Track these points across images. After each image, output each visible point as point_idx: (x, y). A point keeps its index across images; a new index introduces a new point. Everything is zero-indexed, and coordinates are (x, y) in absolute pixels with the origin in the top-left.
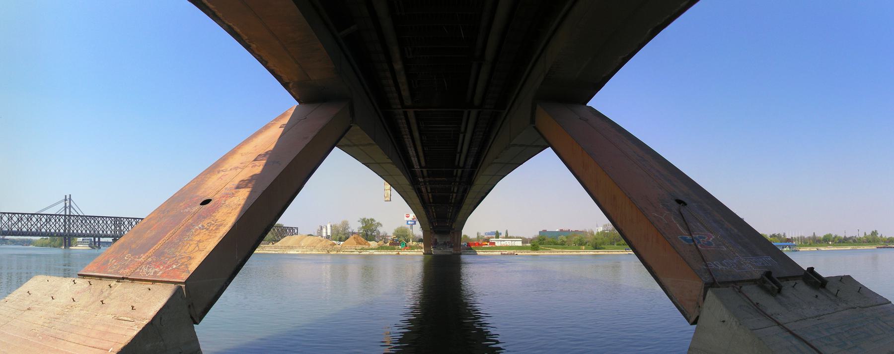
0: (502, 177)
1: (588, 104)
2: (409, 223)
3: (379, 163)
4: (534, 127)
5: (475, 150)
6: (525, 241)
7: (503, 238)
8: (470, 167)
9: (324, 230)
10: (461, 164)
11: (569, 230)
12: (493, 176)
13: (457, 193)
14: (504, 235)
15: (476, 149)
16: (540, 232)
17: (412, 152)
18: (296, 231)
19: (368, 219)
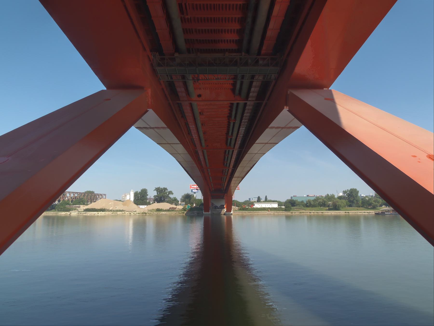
0: (241, 179)
3: (170, 144)
6: (280, 204)
10: (223, 186)
12: (257, 153)
14: (263, 199)
16: (291, 197)
18: (104, 197)
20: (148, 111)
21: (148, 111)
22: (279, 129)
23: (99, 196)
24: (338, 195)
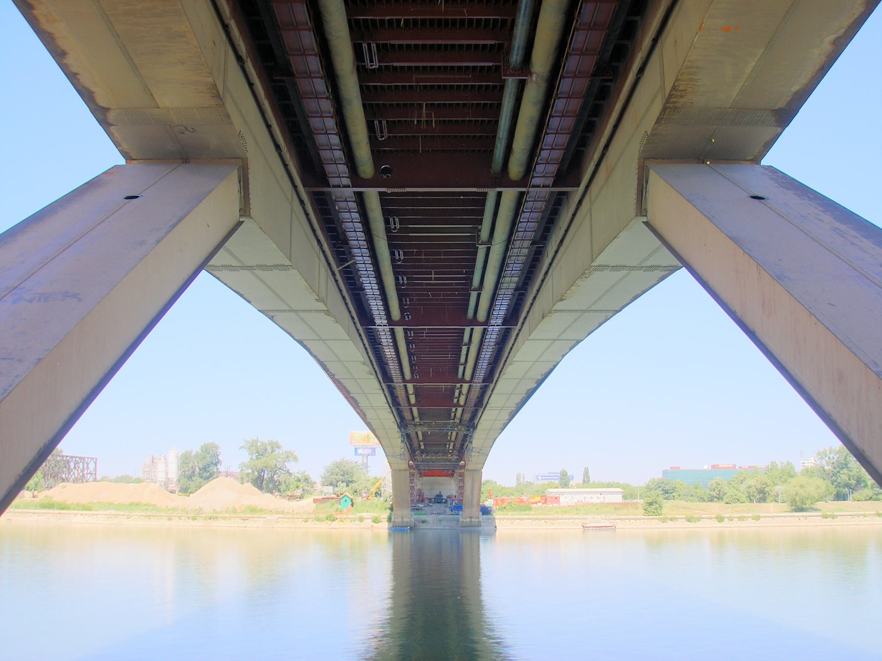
1: (765, 162)
2: (360, 451)
4: (647, 224)
5: (511, 282)
6: (629, 494)
7: (578, 486)
8: (500, 321)
9: (161, 467)
11: (734, 466)
12: (554, 340)
13: (471, 381)
14: (578, 479)
15: (516, 279)
16: (665, 472)
17: (370, 287)
19: (263, 443)
20: (243, 221)
21: (243, 221)
22: (623, 272)
23: (76, 463)
24: (804, 463)
